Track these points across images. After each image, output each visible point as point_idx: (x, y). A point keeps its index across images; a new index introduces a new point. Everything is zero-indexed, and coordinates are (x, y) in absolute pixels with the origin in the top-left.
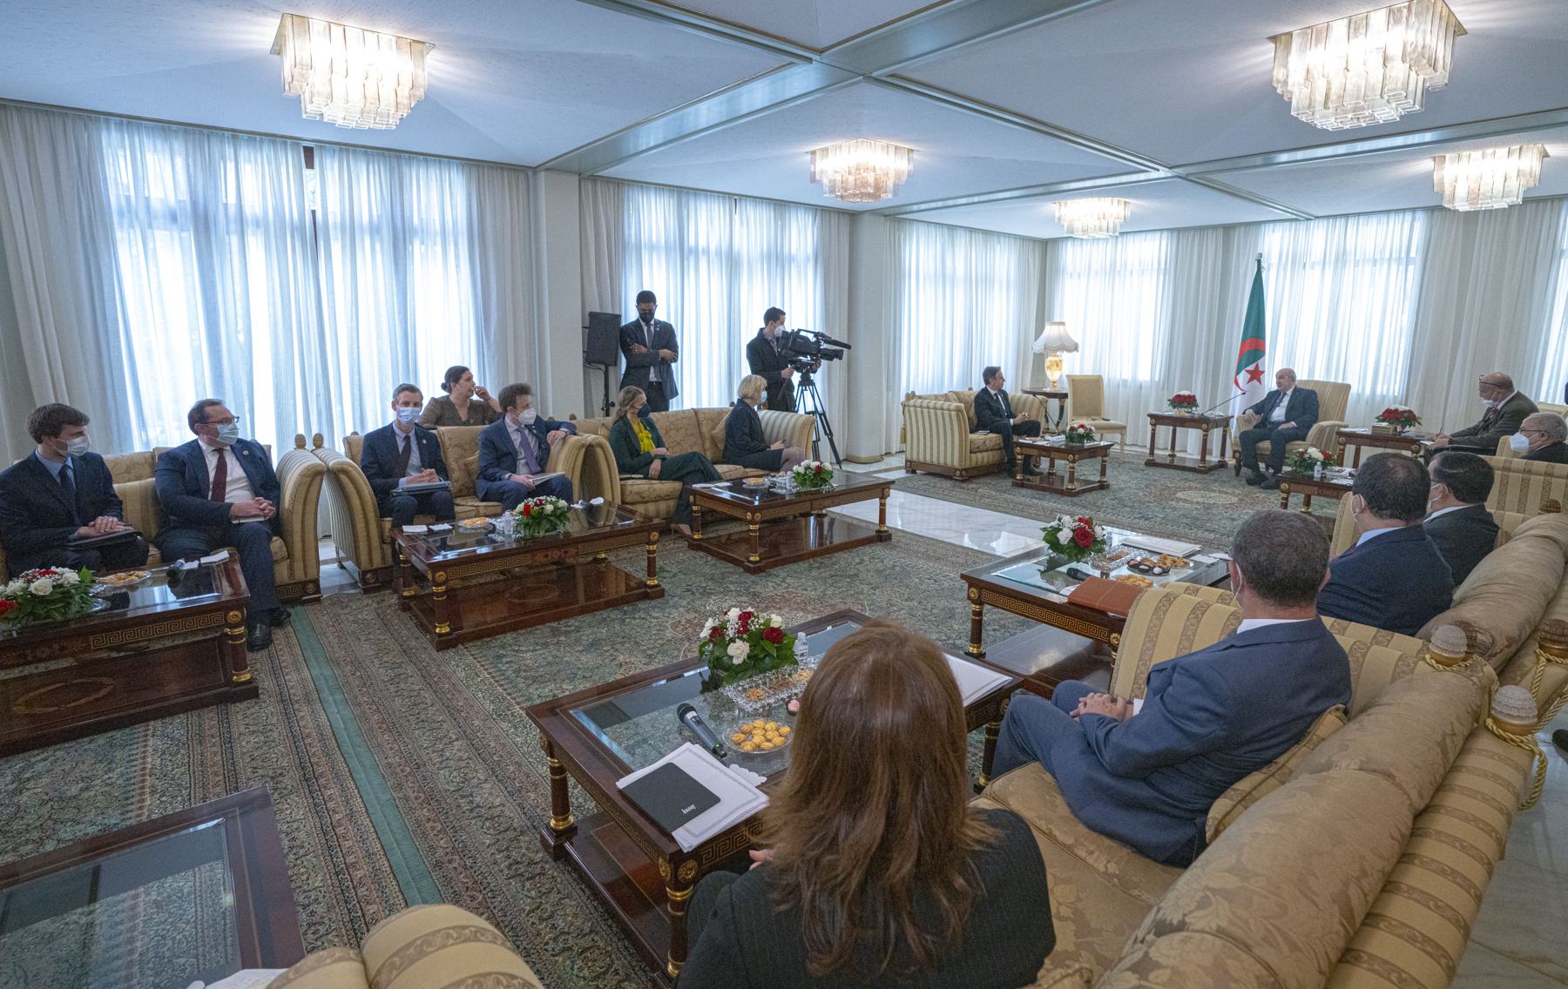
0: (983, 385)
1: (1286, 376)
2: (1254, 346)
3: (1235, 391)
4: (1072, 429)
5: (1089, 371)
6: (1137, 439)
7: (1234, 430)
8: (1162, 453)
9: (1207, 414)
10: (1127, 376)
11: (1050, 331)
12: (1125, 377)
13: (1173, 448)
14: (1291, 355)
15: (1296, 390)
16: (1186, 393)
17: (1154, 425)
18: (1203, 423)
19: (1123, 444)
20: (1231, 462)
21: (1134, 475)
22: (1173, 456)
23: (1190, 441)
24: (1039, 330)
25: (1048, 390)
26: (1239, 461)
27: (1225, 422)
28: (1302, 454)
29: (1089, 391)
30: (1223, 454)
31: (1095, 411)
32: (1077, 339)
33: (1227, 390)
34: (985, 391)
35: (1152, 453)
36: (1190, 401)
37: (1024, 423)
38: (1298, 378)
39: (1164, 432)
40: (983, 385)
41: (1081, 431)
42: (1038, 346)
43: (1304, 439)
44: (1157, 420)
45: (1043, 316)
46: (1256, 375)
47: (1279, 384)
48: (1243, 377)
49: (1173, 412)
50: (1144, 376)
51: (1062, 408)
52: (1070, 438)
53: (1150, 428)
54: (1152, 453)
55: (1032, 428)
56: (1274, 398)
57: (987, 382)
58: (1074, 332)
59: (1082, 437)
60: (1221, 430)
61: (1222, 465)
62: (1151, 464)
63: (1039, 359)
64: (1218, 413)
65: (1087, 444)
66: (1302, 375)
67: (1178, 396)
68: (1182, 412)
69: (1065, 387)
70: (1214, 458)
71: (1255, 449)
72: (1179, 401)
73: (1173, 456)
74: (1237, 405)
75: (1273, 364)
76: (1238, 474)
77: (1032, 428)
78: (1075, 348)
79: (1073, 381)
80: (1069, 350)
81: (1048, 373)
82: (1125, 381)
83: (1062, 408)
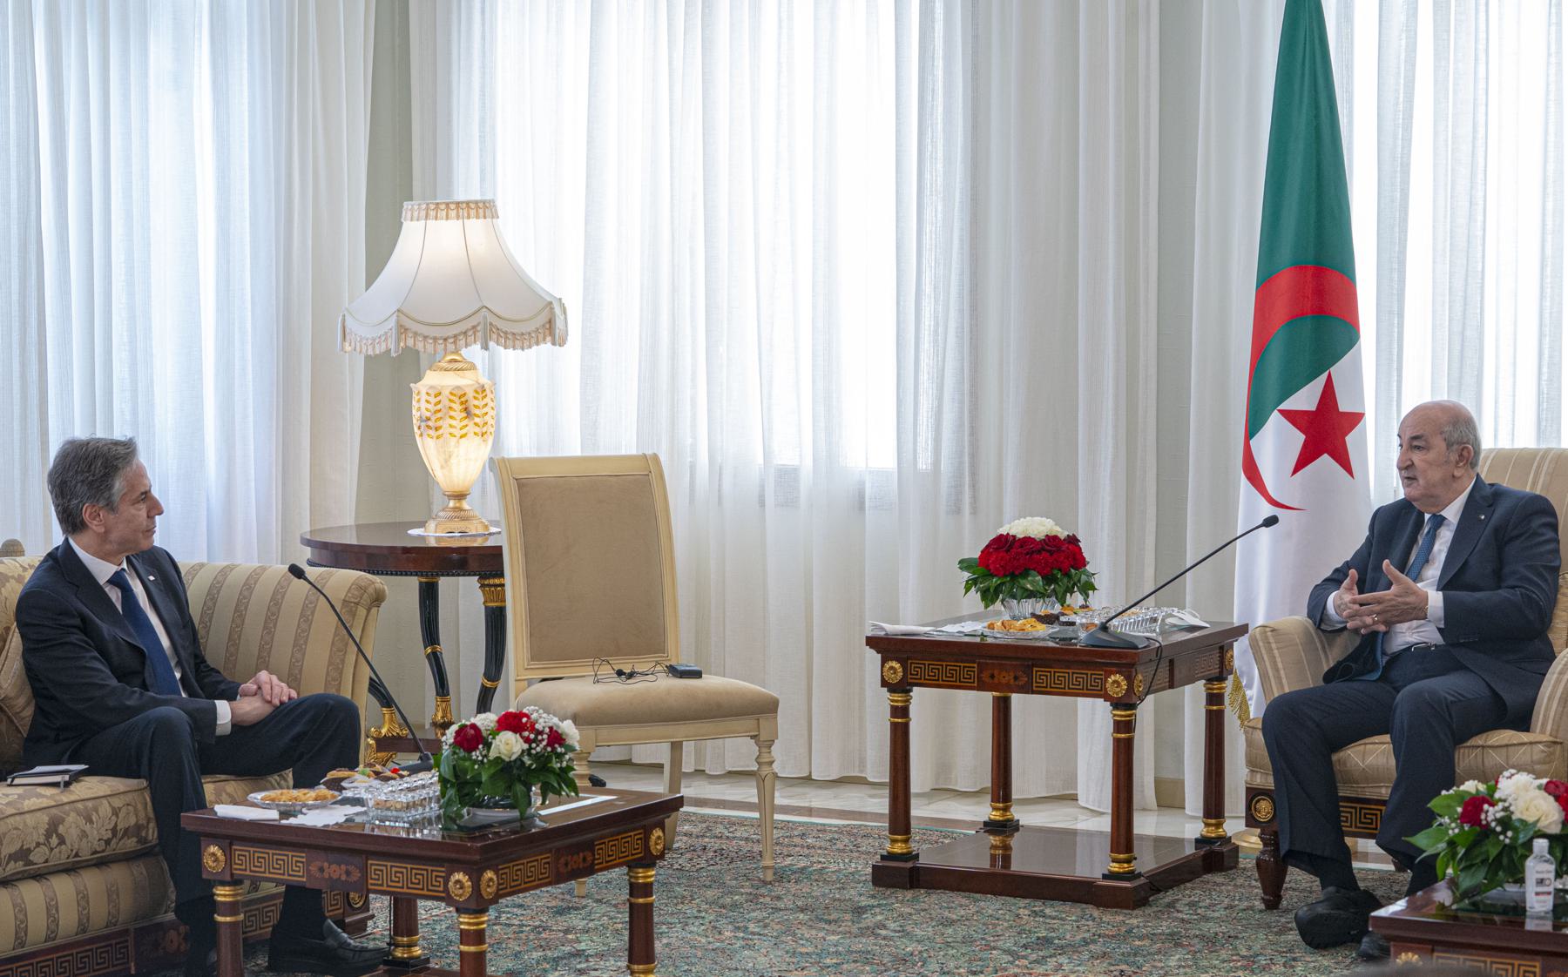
0: (58, 538)
1: (1441, 436)
2: (1309, 299)
3: (1249, 506)
4: (470, 739)
5: (621, 439)
6: (825, 761)
7: (1253, 691)
8: (951, 814)
9: (1131, 627)
10: (794, 448)
11: (429, 245)
12: (786, 456)
13: (1001, 789)
14: (1463, 345)
15: (1485, 499)
16: (1036, 526)
17: (900, 687)
18: (1109, 667)
19: (761, 776)
20: (1251, 842)
21: (812, 937)
22: (1003, 828)
23: (1068, 739)
24: (381, 242)
25: (432, 534)
26: (1271, 839)
27: (1209, 656)
28: (1474, 806)
29: (604, 521)
30: (1214, 808)
31: (628, 624)
32: (567, 288)
33: (1224, 507)
34: (61, 564)
35: (900, 820)
36: (1047, 563)
37: (283, 714)
38: (1487, 442)
39: (952, 720)
40: (58, 538)
41: (509, 745)
42: (370, 315)
43: (1522, 721)
44: (913, 661)
45: (402, 162)
46: (1326, 433)
47: (1408, 471)
48: (1277, 443)
49: (968, 619)
50: (872, 445)
51: (496, 621)
52: (460, 786)
53: (881, 701)
54: (900, 820)
55: (314, 739)
56: (1396, 530)
57: (71, 521)
58: (547, 259)
59: (512, 775)
60: (1192, 697)
61: (1214, 857)
62: (901, 874)
63: (392, 374)
64: (1188, 615)
65: (549, 811)
66: (1506, 430)
67: (1002, 545)
68: (1023, 619)
69: (488, 521)
70: (1173, 827)
71: (1330, 777)
72: (1014, 564)
73: (1003, 828)
74: (1263, 585)
75: (1390, 376)
76: (1273, 901)
77: (314, 739)
78: (544, 325)
79: (535, 492)
80: (518, 339)
81: (429, 449)
82: (787, 476)
83: (496, 621)
